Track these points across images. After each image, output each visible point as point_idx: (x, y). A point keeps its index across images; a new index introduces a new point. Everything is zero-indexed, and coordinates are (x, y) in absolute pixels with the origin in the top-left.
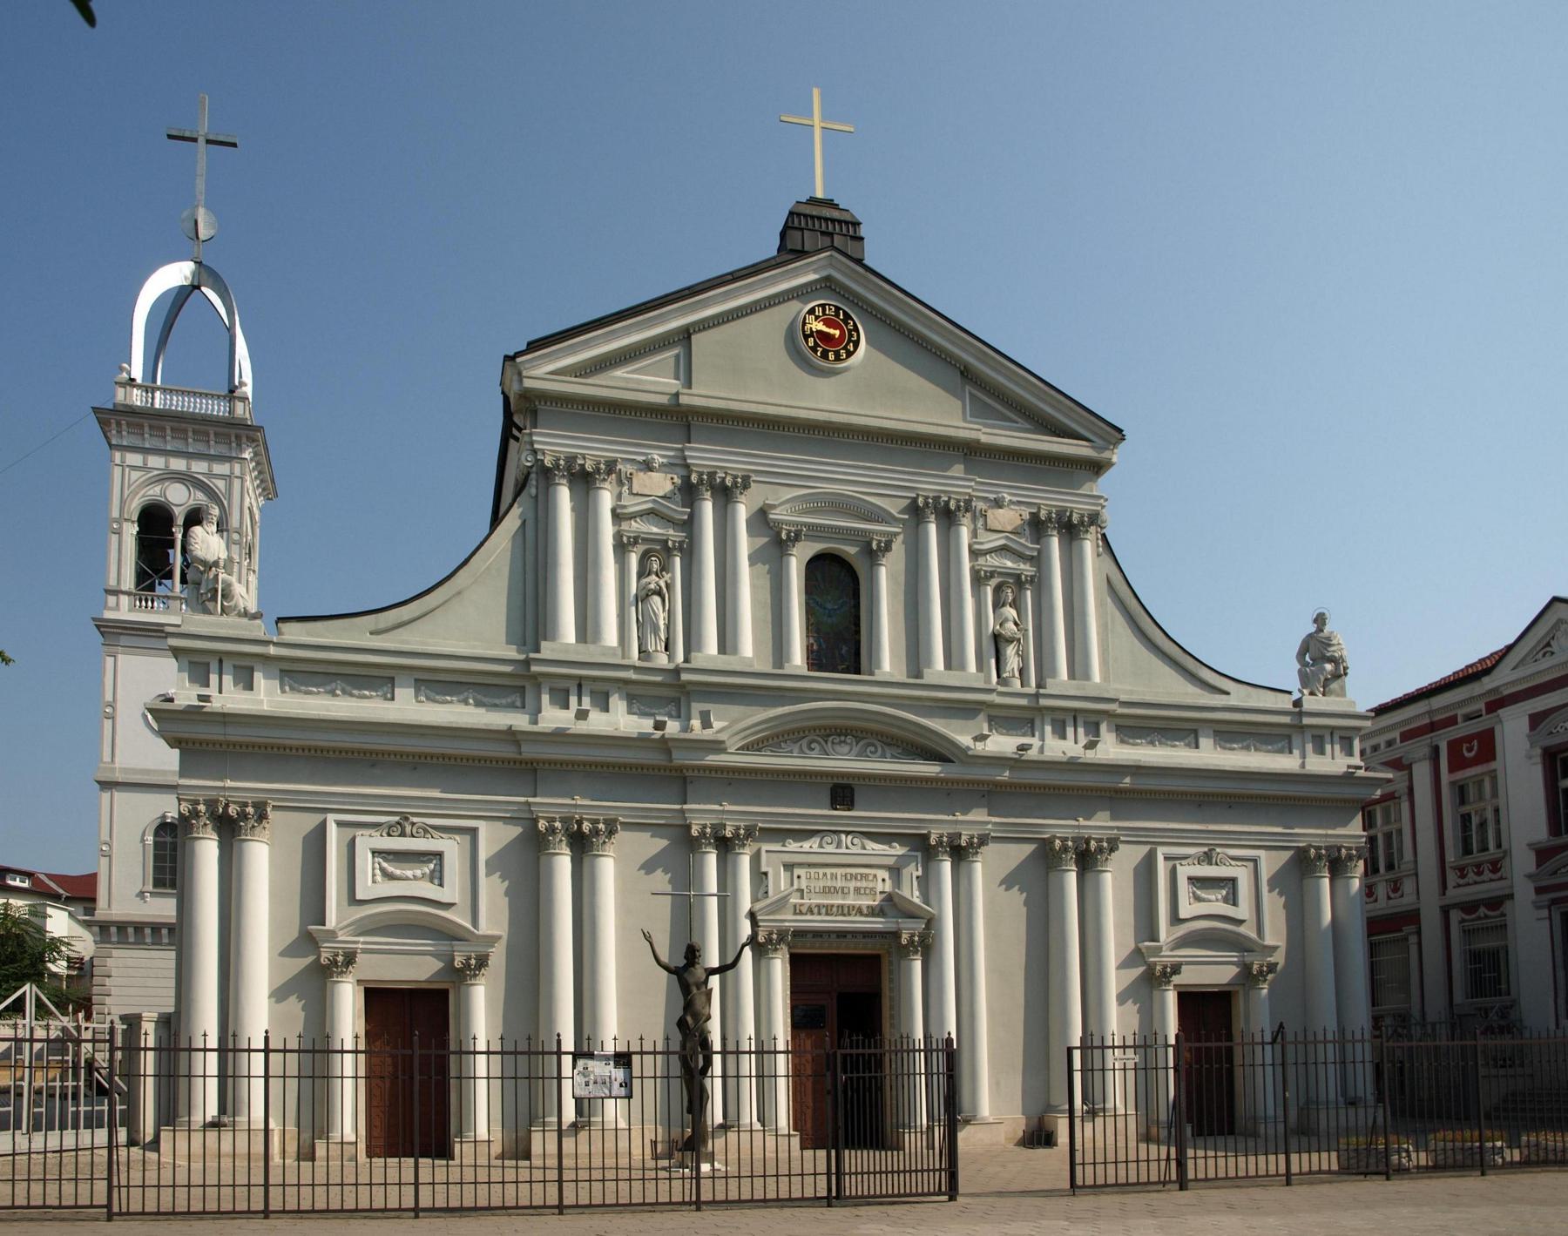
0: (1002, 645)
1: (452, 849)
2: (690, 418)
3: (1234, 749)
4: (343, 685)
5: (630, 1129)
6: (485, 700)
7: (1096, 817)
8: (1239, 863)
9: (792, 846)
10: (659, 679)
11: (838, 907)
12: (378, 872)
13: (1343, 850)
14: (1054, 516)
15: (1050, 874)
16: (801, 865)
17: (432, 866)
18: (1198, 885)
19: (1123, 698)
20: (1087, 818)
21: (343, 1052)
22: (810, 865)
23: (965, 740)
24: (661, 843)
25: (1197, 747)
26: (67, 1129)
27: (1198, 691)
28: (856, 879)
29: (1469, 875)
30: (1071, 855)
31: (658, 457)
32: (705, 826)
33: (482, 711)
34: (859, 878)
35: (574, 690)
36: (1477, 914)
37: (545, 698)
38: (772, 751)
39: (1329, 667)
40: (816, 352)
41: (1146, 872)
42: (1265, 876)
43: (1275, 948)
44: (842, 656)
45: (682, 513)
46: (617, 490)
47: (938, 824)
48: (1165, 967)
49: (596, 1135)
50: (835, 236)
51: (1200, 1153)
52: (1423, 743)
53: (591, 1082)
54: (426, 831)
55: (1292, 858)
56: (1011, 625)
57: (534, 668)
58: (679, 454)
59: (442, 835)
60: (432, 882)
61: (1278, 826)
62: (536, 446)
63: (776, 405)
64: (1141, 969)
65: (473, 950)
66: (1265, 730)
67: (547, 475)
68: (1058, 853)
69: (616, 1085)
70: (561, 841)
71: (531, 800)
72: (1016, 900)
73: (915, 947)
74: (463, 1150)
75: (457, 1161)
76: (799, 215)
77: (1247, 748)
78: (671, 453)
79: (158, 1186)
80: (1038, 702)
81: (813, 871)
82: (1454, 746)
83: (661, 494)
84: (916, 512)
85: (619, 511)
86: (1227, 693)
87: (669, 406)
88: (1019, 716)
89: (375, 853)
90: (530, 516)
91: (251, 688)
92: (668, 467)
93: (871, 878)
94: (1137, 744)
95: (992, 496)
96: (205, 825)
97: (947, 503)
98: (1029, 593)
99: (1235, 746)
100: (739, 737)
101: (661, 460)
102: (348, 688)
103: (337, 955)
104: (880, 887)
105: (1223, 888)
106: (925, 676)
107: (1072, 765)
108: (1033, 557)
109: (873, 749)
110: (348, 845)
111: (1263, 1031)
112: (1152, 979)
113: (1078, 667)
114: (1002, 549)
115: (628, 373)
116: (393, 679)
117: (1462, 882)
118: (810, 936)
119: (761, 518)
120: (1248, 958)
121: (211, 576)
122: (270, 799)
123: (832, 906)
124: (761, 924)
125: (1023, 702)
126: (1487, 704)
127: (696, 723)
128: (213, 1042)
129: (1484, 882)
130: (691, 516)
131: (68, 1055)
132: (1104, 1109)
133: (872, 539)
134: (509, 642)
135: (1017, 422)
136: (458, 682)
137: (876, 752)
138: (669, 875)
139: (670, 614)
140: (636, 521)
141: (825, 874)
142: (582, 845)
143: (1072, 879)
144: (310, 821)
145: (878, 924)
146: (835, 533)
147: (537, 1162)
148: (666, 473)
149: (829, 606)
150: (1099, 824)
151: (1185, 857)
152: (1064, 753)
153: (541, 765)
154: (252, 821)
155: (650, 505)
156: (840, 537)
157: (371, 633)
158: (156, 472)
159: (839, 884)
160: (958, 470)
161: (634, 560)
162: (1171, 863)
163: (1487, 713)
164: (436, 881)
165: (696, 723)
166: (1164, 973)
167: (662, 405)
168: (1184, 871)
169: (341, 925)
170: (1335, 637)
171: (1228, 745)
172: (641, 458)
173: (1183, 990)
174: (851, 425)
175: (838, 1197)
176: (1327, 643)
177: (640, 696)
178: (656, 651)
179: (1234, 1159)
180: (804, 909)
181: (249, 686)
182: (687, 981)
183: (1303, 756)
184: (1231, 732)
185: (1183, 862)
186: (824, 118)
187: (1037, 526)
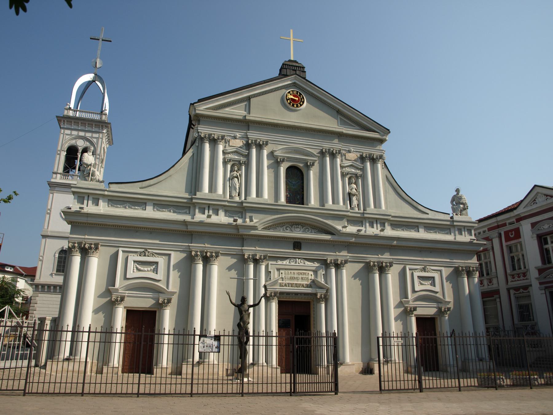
0: (351, 197)
1: (161, 261)
3: (431, 233)
5: (218, 364)
6: (177, 211)
9: (280, 262)
10: (236, 205)
11: (295, 284)
12: (135, 268)
16: (282, 269)
17: (154, 267)
19: (393, 215)
21: (117, 333)
22: (286, 269)
23: (339, 227)
24: (235, 260)
25: (419, 232)
27: (418, 213)
30: (377, 268)
31: (238, 135)
33: (175, 214)
35: (207, 208)
36: (520, 291)
37: (197, 211)
38: (273, 230)
39: (462, 206)
41: (403, 274)
42: (444, 276)
43: (449, 302)
45: (245, 152)
47: (330, 256)
48: (411, 308)
53: (205, 346)
54: (153, 255)
56: (354, 190)
57: (194, 201)
59: (159, 256)
62: (199, 131)
64: (403, 309)
65: (166, 297)
69: (214, 347)
73: (322, 299)
74: (157, 371)
77: (436, 232)
80: (364, 215)
81: (287, 271)
82: (506, 233)
83: (239, 146)
84: (322, 154)
86: (428, 214)
89: (135, 262)
90: (196, 152)
93: (307, 274)
94: (398, 230)
95: (347, 149)
97: (333, 151)
99: (432, 231)
104: (310, 277)
105: (430, 280)
106: (326, 206)
107: (376, 237)
108: (361, 168)
109: (308, 230)
111: (469, 332)
112: (406, 313)
113: (377, 204)
115: (230, 109)
116: (146, 203)
117: (513, 280)
118: (285, 294)
119: (271, 154)
121: (89, 169)
123: (293, 284)
124: (268, 290)
125: (359, 215)
128: (70, 328)
129: (521, 280)
130: (363, 167)
132: (391, 360)
134: (186, 192)
138: (237, 272)
141: (291, 273)
142: (207, 260)
143: (377, 276)
144: (113, 250)
145: (309, 290)
147: (104, 375)
148: (241, 140)
150: (386, 257)
152: (373, 233)
155: (235, 150)
157: (140, 188)
158: (74, 136)
159: (296, 276)
160: (336, 141)
161: (229, 166)
162: (411, 271)
163: (516, 222)
164: (155, 272)
165: (248, 220)
166: (411, 310)
167: (240, 119)
168: (416, 274)
169: (120, 287)
171: (429, 231)
172: (233, 135)
175: (294, 392)
176: (460, 198)
177: (229, 211)
180: (283, 285)
181: (217, 215)
183: (455, 235)
184: (430, 227)
185: (416, 271)
186: (294, 38)
187: (362, 159)
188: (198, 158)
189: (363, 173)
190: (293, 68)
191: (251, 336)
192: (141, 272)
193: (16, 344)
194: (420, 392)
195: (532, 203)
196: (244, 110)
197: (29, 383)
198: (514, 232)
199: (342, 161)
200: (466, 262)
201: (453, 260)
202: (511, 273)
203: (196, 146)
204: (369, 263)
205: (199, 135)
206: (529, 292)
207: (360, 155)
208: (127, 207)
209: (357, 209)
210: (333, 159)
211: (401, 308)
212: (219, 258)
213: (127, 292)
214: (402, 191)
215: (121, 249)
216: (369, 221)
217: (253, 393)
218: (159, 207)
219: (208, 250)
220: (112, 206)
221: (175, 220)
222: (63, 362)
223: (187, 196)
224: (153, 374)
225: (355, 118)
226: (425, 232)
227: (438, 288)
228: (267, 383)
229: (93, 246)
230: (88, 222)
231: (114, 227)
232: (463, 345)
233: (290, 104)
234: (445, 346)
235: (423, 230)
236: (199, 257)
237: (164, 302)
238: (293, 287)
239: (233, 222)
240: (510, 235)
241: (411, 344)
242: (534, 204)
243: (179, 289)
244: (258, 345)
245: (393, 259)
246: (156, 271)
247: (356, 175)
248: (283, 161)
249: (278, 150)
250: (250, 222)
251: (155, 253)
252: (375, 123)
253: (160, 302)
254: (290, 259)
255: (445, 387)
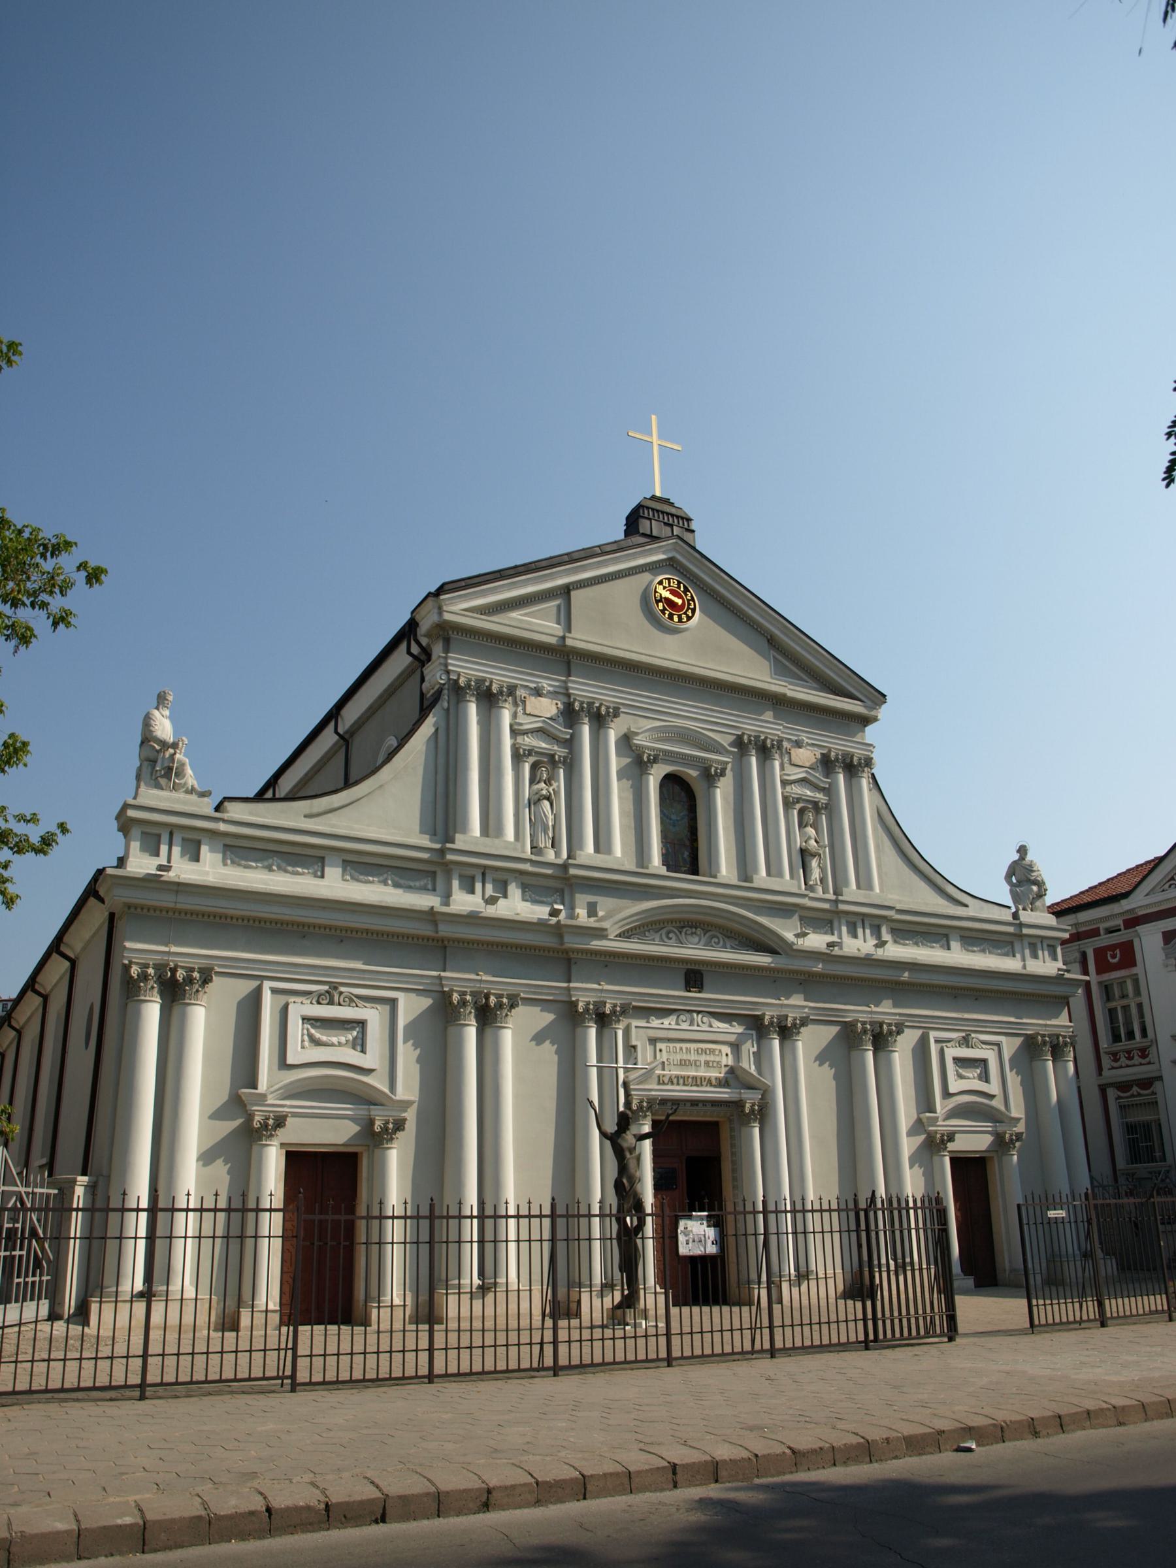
0: (807, 858)
1: (374, 1016)
2: (571, 657)
4: (279, 861)
5: (530, 1290)
6: (402, 882)
7: (883, 1004)
8: (988, 1047)
9: (655, 1022)
10: (549, 872)
11: (693, 1078)
12: (306, 1038)
13: (885, 1026)
14: (473, 683)
15: (449, 1028)
16: (662, 1040)
17: (355, 1033)
18: (959, 1064)
19: (898, 906)
20: (876, 1006)
22: (670, 1040)
23: (789, 936)
24: (549, 1017)
25: (949, 949)
26: (10, 1302)
28: (706, 1053)
29: (1121, 1060)
30: (869, 1037)
31: (546, 685)
32: (588, 1003)
33: (400, 891)
34: (708, 1052)
35: (479, 877)
36: (1131, 1092)
37: (455, 883)
38: (639, 939)
39: (1035, 888)
40: (664, 614)
41: (921, 1051)
42: (1007, 1057)
43: (1018, 1120)
44: (684, 860)
45: (565, 733)
46: (513, 709)
47: (770, 1007)
48: (943, 1135)
49: (501, 1297)
50: (675, 527)
51: (1041, 1302)
52: (1074, 948)
53: (691, 1240)
54: (351, 1000)
55: (1023, 1043)
56: (812, 842)
57: (450, 857)
58: (562, 685)
59: (366, 1005)
60: (354, 1048)
61: (1010, 1016)
62: (450, 668)
63: (649, 656)
64: (923, 1137)
65: (393, 1114)
66: (995, 937)
67: (458, 691)
68: (859, 1034)
69: (709, 1243)
70: (153, 987)
71: (443, 974)
72: (827, 1073)
73: (754, 1115)
74: (380, 1317)
75: (374, 1327)
76: (643, 506)
77: (983, 951)
78: (557, 684)
79: (265, 1350)
80: (837, 907)
81: (671, 1045)
82: (1100, 953)
83: (549, 716)
84: (740, 744)
85: (516, 727)
86: (966, 906)
87: (558, 646)
88: (821, 917)
89: (305, 1019)
90: (443, 725)
91: (197, 860)
92: (553, 695)
93: (717, 1053)
94: (906, 945)
95: (794, 738)
96: (153, 987)
97: (599, 708)
98: (824, 817)
99: (975, 949)
100: (617, 926)
101: (549, 688)
102: (284, 865)
103: (268, 1119)
104: (724, 1062)
105: (977, 1067)
106: (755, 881)
107: (868, 961)
108: (825, 788)
109: (716, 940)
110: (282, 1008)
111: (1060, 1193)
112: (933, 1145)
113: (864, 881)
114: (538, 731)
115: (521, 615)
117: (1115, 1065)
118: (669, 1104)
119: (626, 740)
120: (375, 1111)
121: (167, 755)
122: (217, 965)
123: (688, 1077)
124: (633, 1093)
125: (826, 906)
126: (1124, 921)
127: (581, 912)
128: (144, 1204)
129: (1134, 1065)
130: (572, 735)
131: (18, 1223)
132: (495, 1284)
133: (644, 752)
134: (422, 832)
135: (807, 682)
136: (378, 865)
137: (719, 943)
138: (556, 1046)
139: (556, 818)
140: (528, 737)
141: (681, 1049)
142: (487, 1016)
143: (471, 1033)
144: (245, 987)
145: (724, 1094)
146: (682, 759)
147: (244, 1333)
148: (552, 699)
149: (674, 817)
150: (885, 1010)
151: (949, 1041)
152: (859, 950)
153: (451, 942)
154: (197, 986)
156: (686, 762)
157: (305, 816)
159: (693, 1057)
160: (768, 715)
162: (940, 1045)
163: (1125, 929)
164: (359, 1048)
165: (581, 912)
166: (942, 1141)
167: (551, 644)
168: (951, 1052)
169: (272, 1089)
170: (1035, 864)
171: (970, 948)
172: (533, 685)
173: (954, 1155)
174: (533, 640)
175: (876, 1340)
176: (1030, 869)
177: (534, 887)
178: (546, 847)
179: (1071, 1304)
180: (666, 1080)
181: (196, 858)
182: (620, 1145)
184: (976, 938)
185: (949, 1045)
186: (660, 437)
187: (827, 763)
188: (451, 742)
189: (571, 752)
190: (666, 518)
191: (649, 1215)
192: (322, 1048)
193: (15, 1256)
194: (668, 1366)
195: (1167, 886)
196: (554, 618)
197: (286, 1349)
198: (1120, 951)
199: (515, 715)
200: (1049, 1022)
201: (1021, 1019)
202: (1110, 1050)
203: (443, 709)
204: (881, 1024)
205: (449, 679)
206: (1156, 1094)
207: (821, 754)
208: (275, 868)
209: (820, 889)
210: (765, 761)
211: (919, 1135)
212: (210, 987)
213: (288, 1102)
214: (912, 849)
215: (267, 985)
216: (847, 922)
217: (703, 1356)
218: (356, 871)
219: (180, 962)
220: (233, 862)
221: (408, 907)
222: (132, 1302)
223: (425, 841)
224: (370, 1326)
225: (813, 663)
226: (225, 864)
227: (994, 1087)
228: (495, 1346)
229: (196, 975)
230: (179, 906)
231: (246, 922)
232: (1035, 1224)
233: (663, 611)
234: (749, 1237)
235: (959, 944)
236: (469, 1009)
237: (385, 1129)
238: (687, 1085)
239: (547, 917)
240: (1109, 958)
241: (750, 1230)
242: (1170, 886)
243: (418, 1096)
244: (495, 1241)
245: (900, 1015)
246: (360, 1044)
247: (552, 756)
248: (655, 760)
249: (642, 733)
250: (589, 916)
251: (358, 997)
252: (855, 677)
253: (377, 1128)
254: (678, 1013)
255: (1070, 1320)
